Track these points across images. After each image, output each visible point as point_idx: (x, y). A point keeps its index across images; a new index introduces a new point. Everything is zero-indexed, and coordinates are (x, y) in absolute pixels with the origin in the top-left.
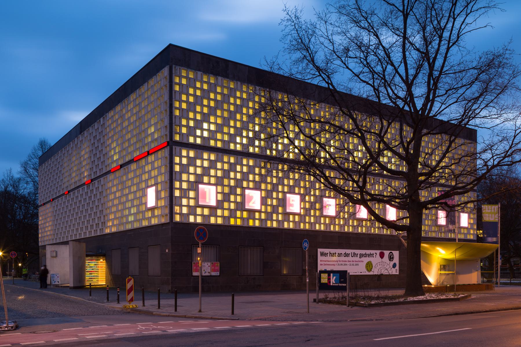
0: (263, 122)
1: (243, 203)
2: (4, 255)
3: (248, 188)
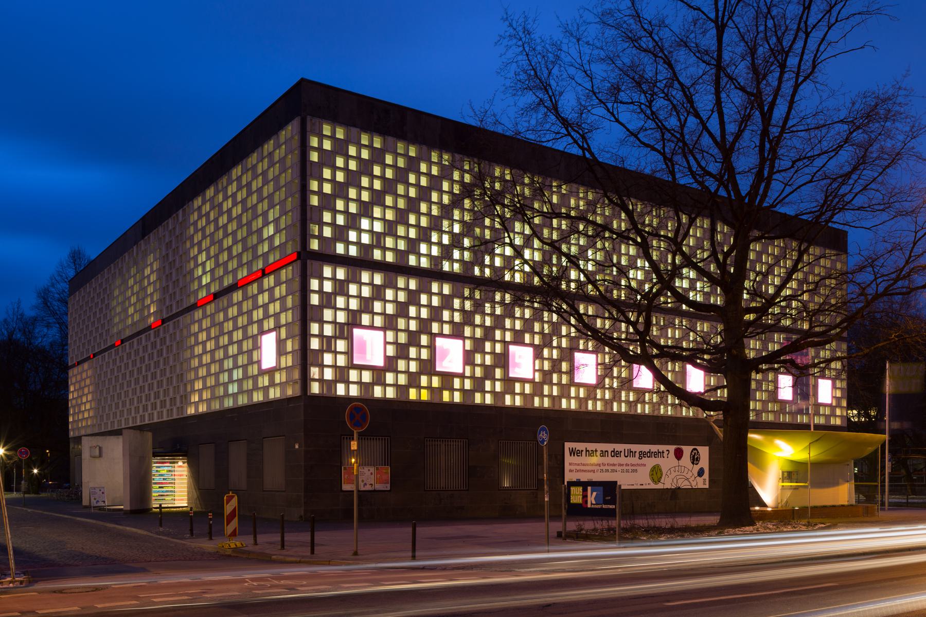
1: (432, 360)
3: (441, 335)
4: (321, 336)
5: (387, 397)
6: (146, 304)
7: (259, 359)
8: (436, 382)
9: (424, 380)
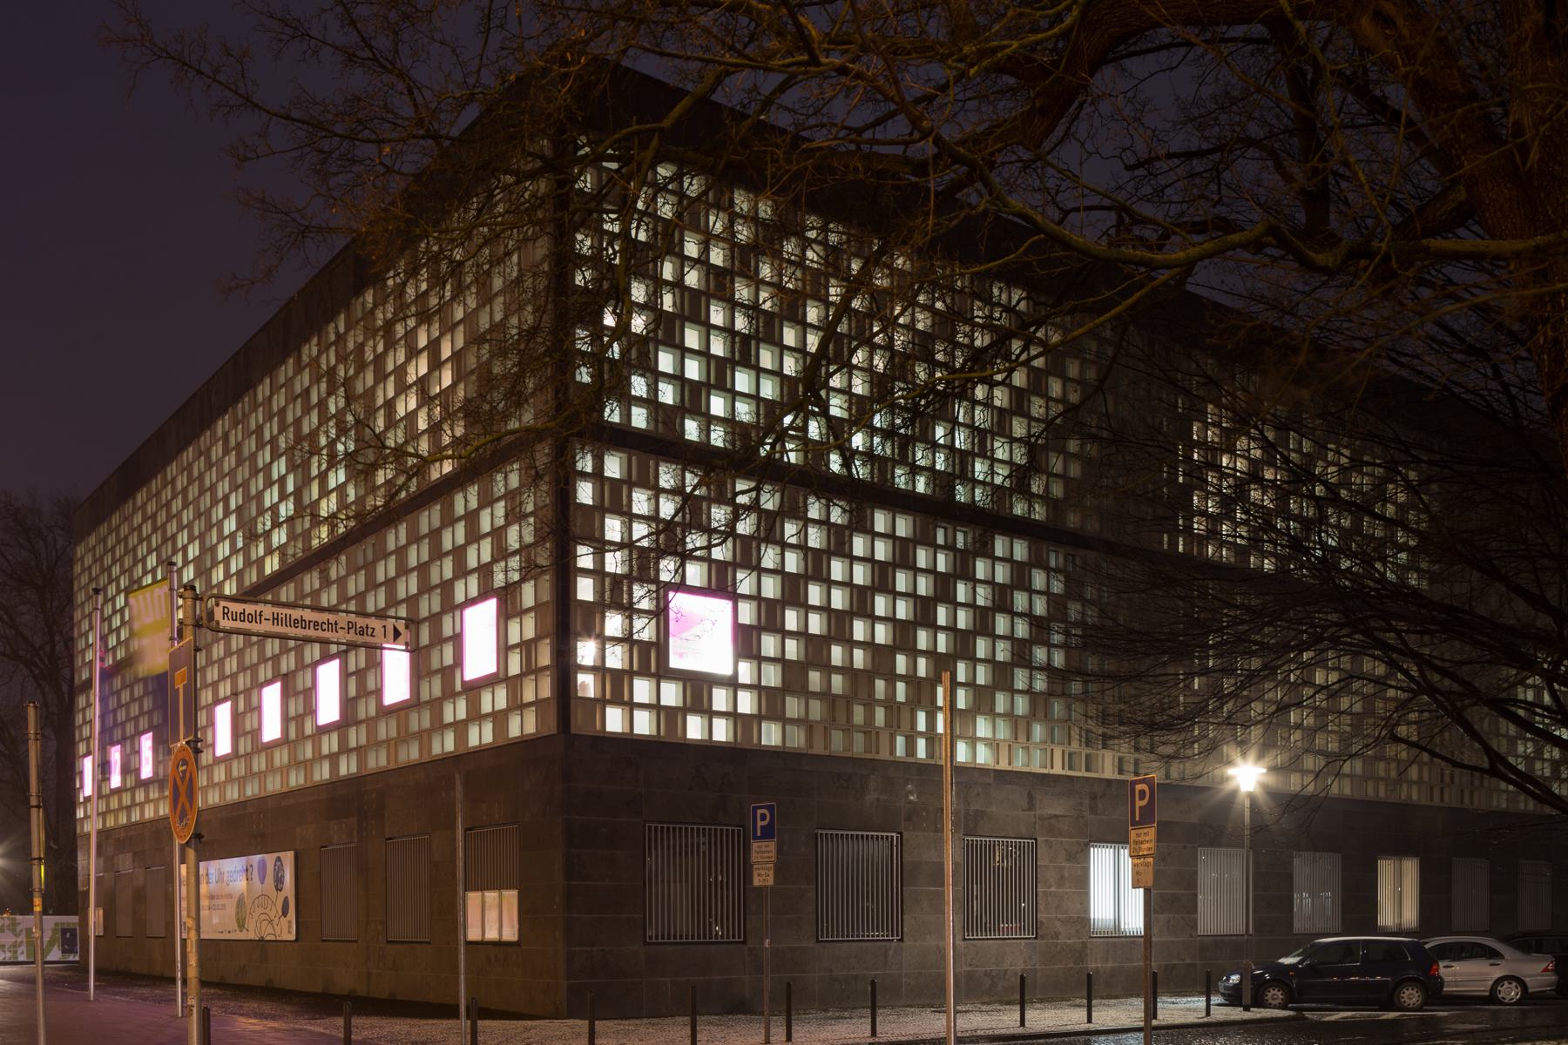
0: (741, 323)
1: (660, 646)
2: (1295, 783)
3: (682, 587)
4: (598, 573)
5: (636, 732)
6: (214, 582)
7: (458, 630)
8: (671, 694)
9: (642, 690)
